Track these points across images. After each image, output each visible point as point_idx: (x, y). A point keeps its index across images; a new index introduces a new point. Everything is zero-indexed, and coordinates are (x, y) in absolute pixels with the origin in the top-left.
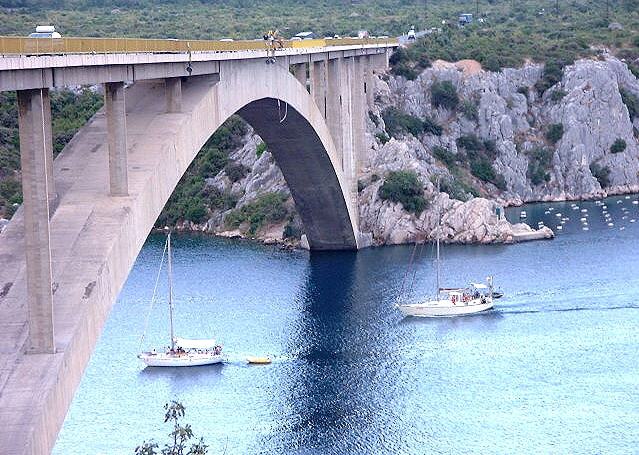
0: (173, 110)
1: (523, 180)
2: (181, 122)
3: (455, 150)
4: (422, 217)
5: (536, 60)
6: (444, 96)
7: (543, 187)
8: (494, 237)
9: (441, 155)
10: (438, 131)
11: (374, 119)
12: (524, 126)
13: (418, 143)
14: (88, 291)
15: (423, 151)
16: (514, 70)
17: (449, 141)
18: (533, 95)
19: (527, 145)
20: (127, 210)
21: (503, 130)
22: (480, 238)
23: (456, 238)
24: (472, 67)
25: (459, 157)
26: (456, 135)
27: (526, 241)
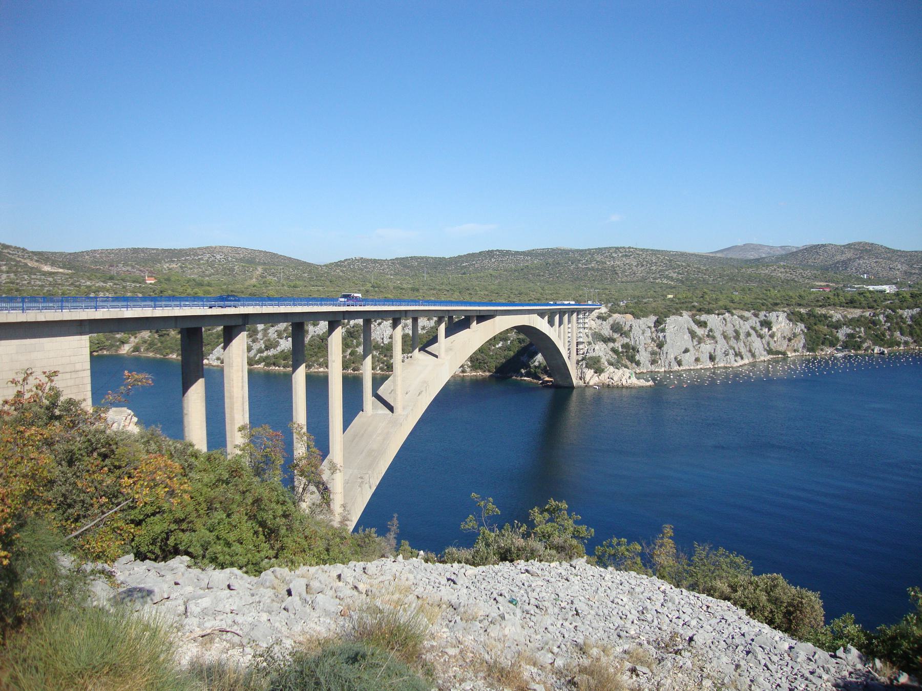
3: (620, 350)
5: (655, 315)
6: (616, 328)
9: (614, 350)
17: (618, 345)
18: (653, 329)
24: (629, 316)
25: (622, 352)
26: (620, 344)
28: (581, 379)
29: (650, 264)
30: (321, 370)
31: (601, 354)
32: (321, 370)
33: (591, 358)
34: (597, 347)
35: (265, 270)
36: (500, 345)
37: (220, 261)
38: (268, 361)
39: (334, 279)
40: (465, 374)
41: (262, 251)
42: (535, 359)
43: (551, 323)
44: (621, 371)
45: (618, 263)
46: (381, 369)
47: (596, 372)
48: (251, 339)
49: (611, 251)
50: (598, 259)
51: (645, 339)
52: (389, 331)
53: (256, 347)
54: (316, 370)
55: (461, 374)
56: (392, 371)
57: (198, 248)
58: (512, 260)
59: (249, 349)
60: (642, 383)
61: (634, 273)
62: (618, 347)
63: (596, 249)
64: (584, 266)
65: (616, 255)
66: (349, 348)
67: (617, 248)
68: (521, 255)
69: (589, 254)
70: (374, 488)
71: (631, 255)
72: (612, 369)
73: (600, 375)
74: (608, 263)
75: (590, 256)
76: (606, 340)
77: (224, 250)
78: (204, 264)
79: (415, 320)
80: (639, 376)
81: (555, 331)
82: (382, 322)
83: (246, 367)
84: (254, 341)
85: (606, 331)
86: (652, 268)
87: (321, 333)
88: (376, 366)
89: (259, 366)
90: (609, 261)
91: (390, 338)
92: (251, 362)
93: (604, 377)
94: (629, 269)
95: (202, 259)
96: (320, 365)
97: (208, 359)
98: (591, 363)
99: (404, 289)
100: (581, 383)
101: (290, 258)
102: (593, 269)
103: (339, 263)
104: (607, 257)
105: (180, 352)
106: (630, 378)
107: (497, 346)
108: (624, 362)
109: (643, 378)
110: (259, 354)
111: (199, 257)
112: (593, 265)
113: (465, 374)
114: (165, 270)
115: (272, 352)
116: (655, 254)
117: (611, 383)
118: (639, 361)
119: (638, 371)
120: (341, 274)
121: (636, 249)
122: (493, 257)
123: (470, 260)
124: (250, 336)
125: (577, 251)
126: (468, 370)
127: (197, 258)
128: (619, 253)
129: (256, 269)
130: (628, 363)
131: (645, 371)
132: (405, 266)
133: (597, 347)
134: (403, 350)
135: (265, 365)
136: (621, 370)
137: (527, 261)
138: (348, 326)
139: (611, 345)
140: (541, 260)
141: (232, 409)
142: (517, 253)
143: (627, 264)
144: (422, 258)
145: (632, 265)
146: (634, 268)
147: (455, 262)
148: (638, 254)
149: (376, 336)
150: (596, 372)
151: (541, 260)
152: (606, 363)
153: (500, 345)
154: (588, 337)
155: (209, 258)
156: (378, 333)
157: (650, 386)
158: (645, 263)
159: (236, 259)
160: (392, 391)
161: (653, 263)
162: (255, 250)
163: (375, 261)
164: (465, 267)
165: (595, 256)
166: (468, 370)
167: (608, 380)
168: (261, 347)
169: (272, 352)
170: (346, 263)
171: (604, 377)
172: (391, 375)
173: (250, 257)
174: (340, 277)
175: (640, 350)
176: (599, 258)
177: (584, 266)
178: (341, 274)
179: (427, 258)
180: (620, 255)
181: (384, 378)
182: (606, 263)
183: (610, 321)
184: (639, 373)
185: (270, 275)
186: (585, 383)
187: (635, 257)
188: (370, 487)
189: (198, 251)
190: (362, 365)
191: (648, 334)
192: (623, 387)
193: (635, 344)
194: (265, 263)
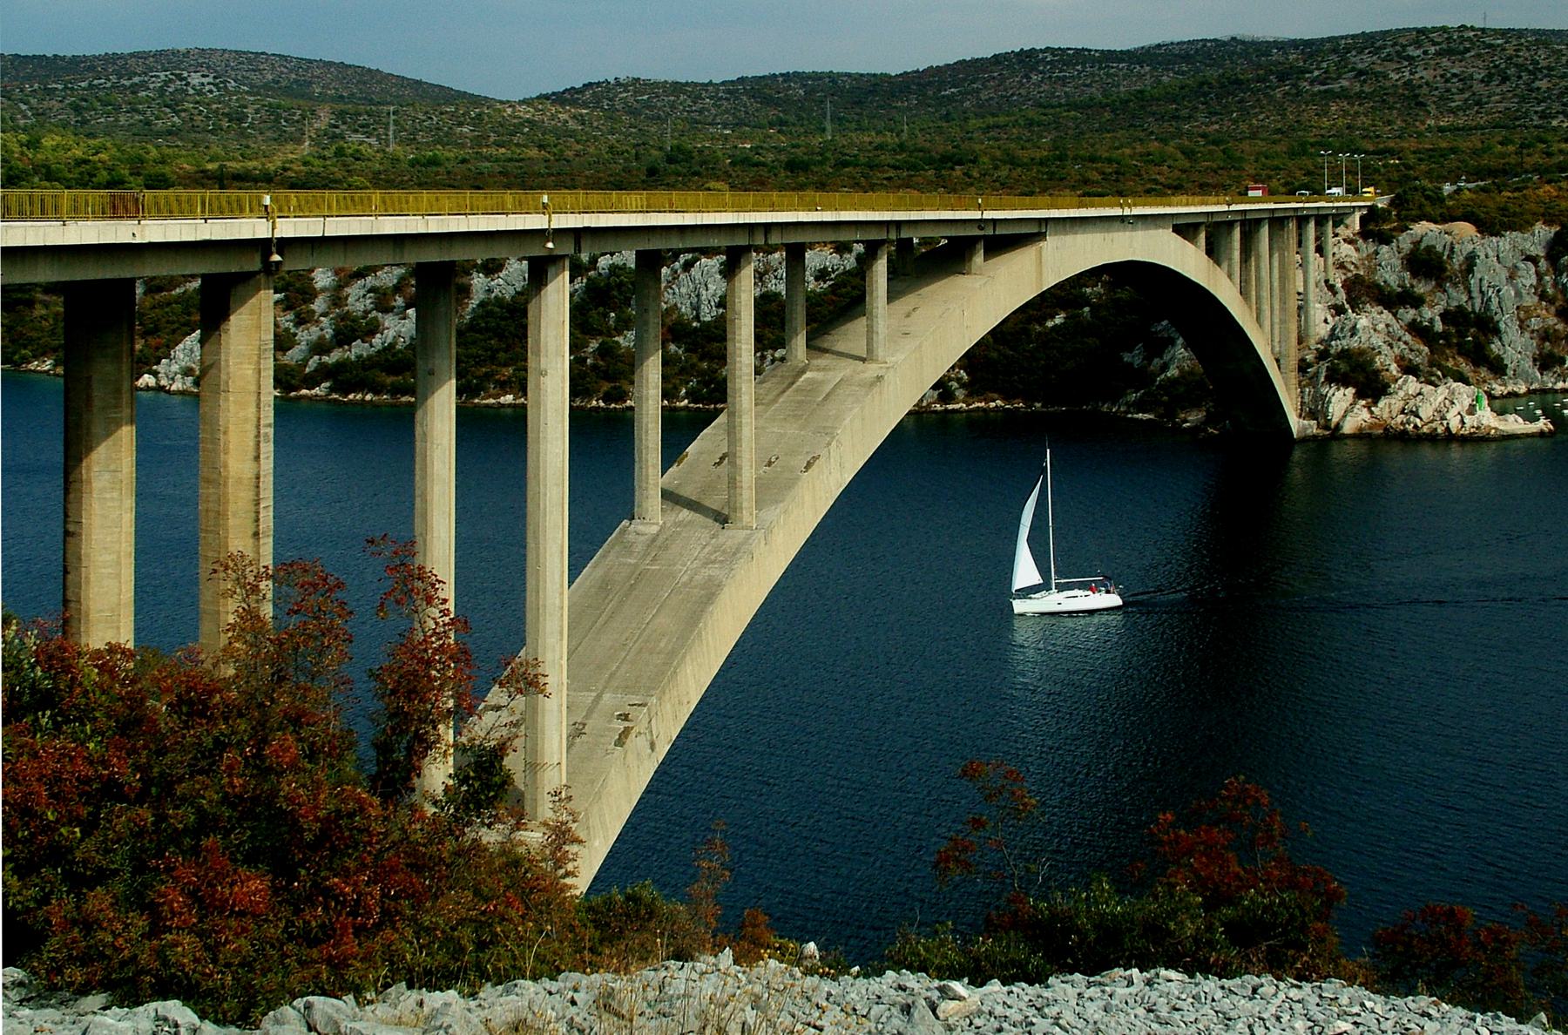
0: (973, 271)
1: (1528, 364)
2: (977, 285)
3: (1439, 326)
4: (1381, 404)
5: (1548, 223)
6: (1424, 263)
7: (1555, 373)
8: (1472, 430)
9: (1415, 328)
10: (1417, 302)
11: (1331, 288)
12: (1530, 300)
13: (1390, 316)
14: (809, 466)
15: (1396, 326)
16: (1520, 235)
17: (1431, 314)
18: (1543, 264)
19: (1534, 323)
20: (879, 378)
21: (1503, 304)
22: (1454, 431)
23: (1425, 430)
24: (1465, 229)
25: (1445, 335)
26: (1439, 309)
27: (67, 491)
28: (1312, 415)
29: (1530, 72)
30: (509, 398)
31: (1377, 340)
32: (509, 398)
33: (1345, 354)
34: (1363, 322)
35: (341, 115)
36: (1059, 320)
37: (199, 93)
38: (342, 377)
39: (551, 139)
40: (950, 407)
41: (331, 64)
42: (1166, 357)
43: (1212, 251)
44: (1442, 391)
45: (1427, 75)
46: (693, 396)
47: (1359, 395)
48: (290, 316)
49: (1403, 41)
50: (1360, 66)
51: (1518, 294)
52: (716, 286)
53: (307, 335)
54: (492, 401)
55: (938, 407)
56: (725, 401)
57: (132, 55)
58: (1093, 75)
59: (283, 342)
60: (1515, 424)
61: (1479, 103)
62: (1431, 321)
63: (1353, 37)
64: (1317, 88)
65: (1418, 52)
66: (594, 336)
67: (1421, 31)
68: (1122, 61)
69: (1335, 51)
70: (663, 749)
71: (1468, 50)
72: (1412, 385)
73: (1375, 403)
74: (1394, 76)
75: (1334, 57)
76: (1391, 300)
77: (215, 59)
78: (149, 100)
79: (795, 254)
80: (1501, 405)
81: (1230, 276)
82: (697, 260)
83: (270, 393)
84: (301, 321)
85: (1391, 272)
86: (1537, 84)
87: (508, 293)
88: (677, 389)
89: (316, 391)
90: (1398, 70)
91: (719, 305)
92: (285, 379)
93: (1388, 408)
94: (1462, 91)
95: (143, 86)
96: (504, 387)
97: (155, 374)
98: (1343, 367)
99: (764, 165)
100: (1312, 427)
101: (419, 83)
102: (1343, 95)
103: (567, 95)
104: (1388, 59)
105: (61, 354)
106: (1472, 410)
107: (1050, 324)
108: (1450, 364)
109: (1516, 412)
110: (316, 357)
111: (136, 80)
112: (1345, 83)
113: (950, 407)
114: (25, 117)
115: (358, 349)
116: (1546, 45)
117: (1410, 427)
118: (1499, 359)
119: (1498, 389)
120: (572, 125)
121: (1483, 30)
122: (1033, 69)
123: (965, 80)
124: (286, 305)
125: (1295, 44)
126: (960, 394)
127: (127, 83)
128: (1427, 44)
129: (313, 112)
130: (1466, 367)
131: (1522, 389)
132: (767, 101)
133: (1363, 322)
134: (758, 338)
135: (332, 390)
136: (1441, 389)
137: (1141, 76)
138: (592, 273)
139: (1409, 314)
140: (1183, 73)
141: (221, 515)
142: (1109, 56)
143: (1455, 75)
144: (816, 76)
145: (1471, 77)
146: (1478, 87)
147: (919, 84)
148: (1490, 46)
149: (678, 300)
150: (1359, 395)
151: (1183, 73)
152: (1394, 368)
153: (1059, 320)
154: (1335, 293)
155: (167, 83)
156: (683, 290)
157: (1542, 434)
158: (1512, 71)
159: (252, 86)
160: (722, 459)
161: (1540, 70)
162: (310, 61)
163: (677, 88)
164: (951, 99)
165: (1353, 57)
166: (960, 394)
167: (1401, 418)
168: (321, 338)
169: (358, 349)
170: (588, 93)
171: (1388, 408)
172: (722, 410)
173: (296, 81)
174: (572, 134)
175: (1502, 326)
176: (1363, 61)
177: (1317, 88)
178: (572, 125)
179: (832, 77)
180: (1432, 50)
181: (700, 421)
182: (1386, 77)
183: (1405, 241)
184: (1503, 397)
185: (356, 131)
186: (1326, 427)
187: (1479, 56)
188: (652, 746)
189: (132, 61)
190: (632, 383)
191: (1528, 277)
192: (1450, 437)
193: (1487, 308)
194: (342, 97)
